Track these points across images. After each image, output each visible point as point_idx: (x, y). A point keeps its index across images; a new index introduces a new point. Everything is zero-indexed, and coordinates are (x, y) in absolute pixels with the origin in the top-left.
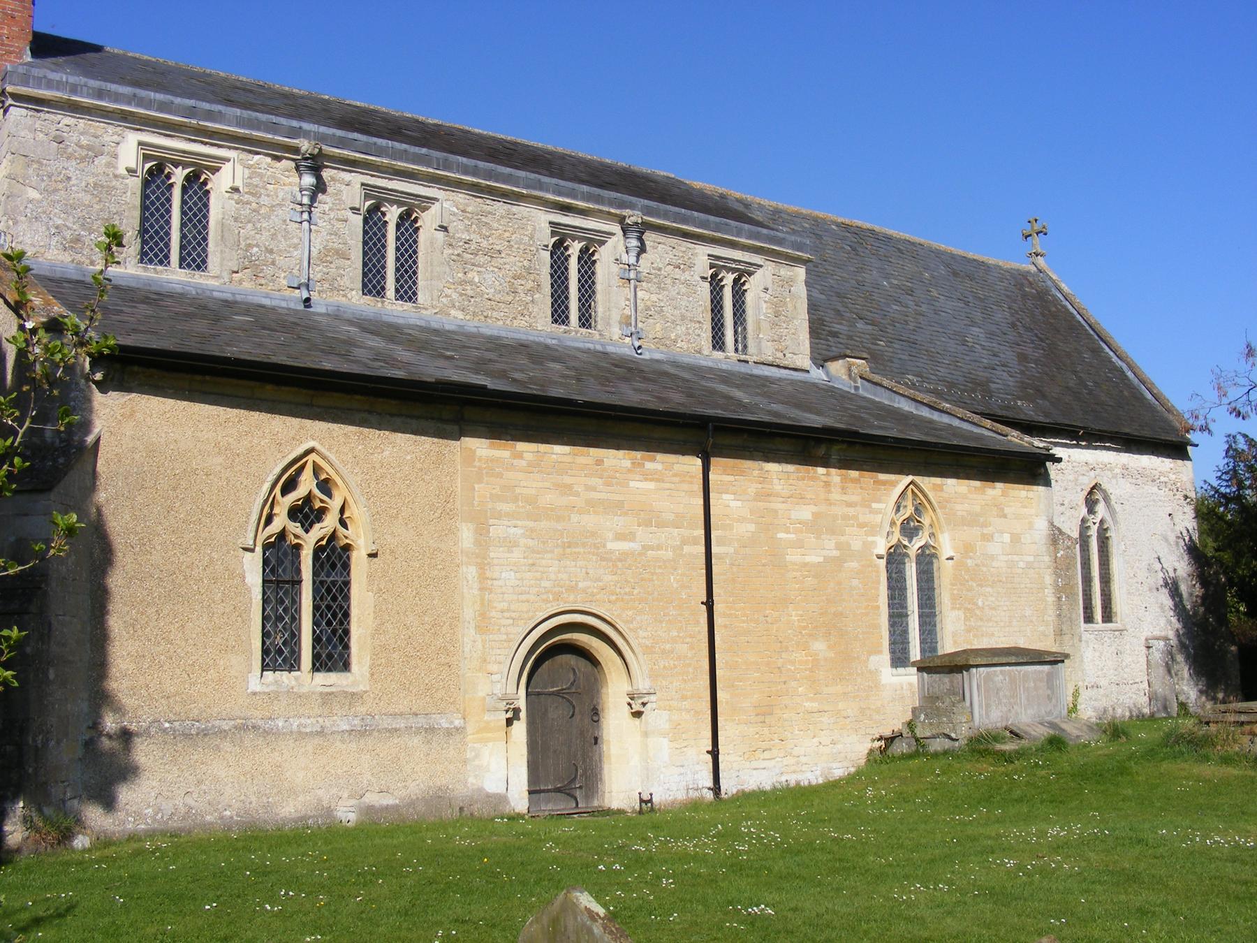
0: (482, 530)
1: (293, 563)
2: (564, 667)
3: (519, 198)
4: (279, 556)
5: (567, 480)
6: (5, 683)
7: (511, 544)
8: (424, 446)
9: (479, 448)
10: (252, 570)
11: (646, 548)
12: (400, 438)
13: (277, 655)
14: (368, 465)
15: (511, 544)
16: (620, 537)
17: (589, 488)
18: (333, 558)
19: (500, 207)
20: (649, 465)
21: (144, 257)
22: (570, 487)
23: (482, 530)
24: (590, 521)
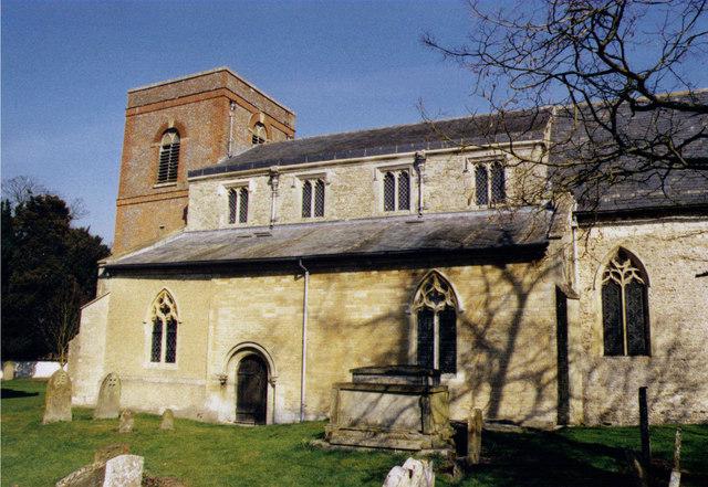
0: (216, 312)
1: (71, 317)
2: (254, 370)
3: (363, 161)
4: (158, 323)
5: (248, 290)
6: (683, 481)
7: (225, 317)
8: (201, 284)
9: (218, 282)
10: (149, 329)
11: (279, 315)
12: (192, 282)
13: (156, 356)
14: (184, 292)
15: (225, 317)
16: (269, 311)
17: (257, 293)
18: (173, 324)
19: (356, 167)
20: (283, 280)
21: (401, 208)
22: (248, 293)
23: (216, 312)
24: (256, 305)
